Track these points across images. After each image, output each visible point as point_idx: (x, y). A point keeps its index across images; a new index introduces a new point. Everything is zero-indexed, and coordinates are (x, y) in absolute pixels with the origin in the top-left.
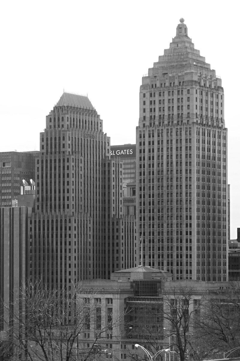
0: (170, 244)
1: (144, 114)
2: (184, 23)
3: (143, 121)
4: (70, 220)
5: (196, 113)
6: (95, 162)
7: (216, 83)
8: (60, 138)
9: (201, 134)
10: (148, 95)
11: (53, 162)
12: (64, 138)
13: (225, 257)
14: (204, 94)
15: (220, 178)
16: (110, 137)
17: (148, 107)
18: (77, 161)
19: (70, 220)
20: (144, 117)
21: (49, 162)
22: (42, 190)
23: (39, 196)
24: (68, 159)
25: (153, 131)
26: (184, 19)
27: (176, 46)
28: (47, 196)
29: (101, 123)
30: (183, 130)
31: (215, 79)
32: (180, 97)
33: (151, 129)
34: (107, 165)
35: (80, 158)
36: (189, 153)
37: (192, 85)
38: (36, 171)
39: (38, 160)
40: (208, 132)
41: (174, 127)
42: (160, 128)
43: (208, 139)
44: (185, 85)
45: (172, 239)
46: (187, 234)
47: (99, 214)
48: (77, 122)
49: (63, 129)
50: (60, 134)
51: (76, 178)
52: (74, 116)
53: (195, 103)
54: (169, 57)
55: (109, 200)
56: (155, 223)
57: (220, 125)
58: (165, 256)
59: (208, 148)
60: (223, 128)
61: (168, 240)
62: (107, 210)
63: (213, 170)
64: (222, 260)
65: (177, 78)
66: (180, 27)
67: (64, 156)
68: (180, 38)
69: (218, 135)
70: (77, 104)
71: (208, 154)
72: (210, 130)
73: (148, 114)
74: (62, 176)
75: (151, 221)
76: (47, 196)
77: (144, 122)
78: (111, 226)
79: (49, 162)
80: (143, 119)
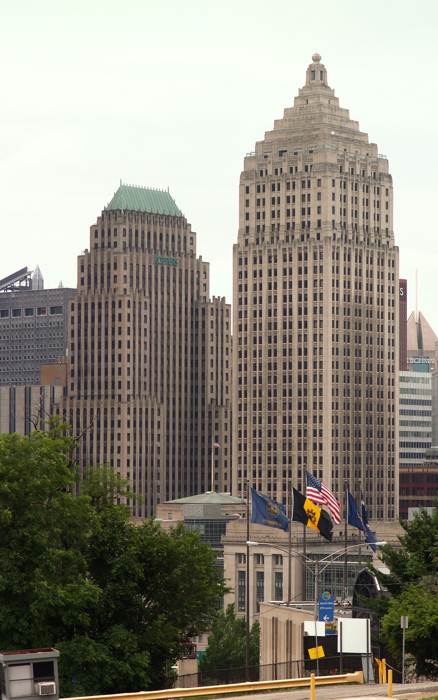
0: (287, 452)
1: (247, 223)
2: (321, 62)
3: (244, 235)
4: (119, 408)
5: (333, 221)
6: (177, 306)
7: (375, 167)
8: (109, 265)
9: (342, 257)
10: (253, 189)
11: (96, 307)
12: (115, 265)
13: (391, 474)
14: (349, 186)
15: (383, 335)
16: (208, 263)
17: (252, 210)
18: (137, 306)
19: (119, 408)
20: (248, 228)
21: (89, 307)
22: (79, 357)
23: (74, 367)
24: (120, 302)
25: (260, 251)
26: (321, 55)
27: (305, 102)
28: (86, 366)
29: (192, 238)
30: (310, 251)
31: (375, 160)
32: (305, 192)
33: (257, 248)
34: (200, 311)
35: (143, 300)
36: (320, 291)
37: (325, 172)
38: (70, 323)
39: (73, 305)
40: (345, 252)
41: (295, 246)
42: (272, 247)
43: (356, 266)
44: (314, 172)
45: (290, 444)
46: (315, 435)
47: (186, 399)
48: (143, 238)
49: (115, 250)
50: (109, 259)
51: (134, 334)
52: (137, 226)
53: (331, 203)
54: (292, 123)
55: (203, 374)
56: (263, 416)
57: (384, 242)
58: (280, 474)
59: (356, 283)
60: (391, 246)
61: (284, 444)
62: (200, 390)
63: (368, 321)
64: (386, 481)
65: (302, 159)
66: (313, 69)
67: (113, 297)
68: (311, 89)
69: (378, 259)
70: (145, 206)
71: (356, 293)
72: (361, 250)
73: (252, 223)
74: (110, 332)
75: (258, 412)
76: (86, 366)
77: (247, 237)
78: (206, 419)
79: (89, 307)
80: (244, 231)
